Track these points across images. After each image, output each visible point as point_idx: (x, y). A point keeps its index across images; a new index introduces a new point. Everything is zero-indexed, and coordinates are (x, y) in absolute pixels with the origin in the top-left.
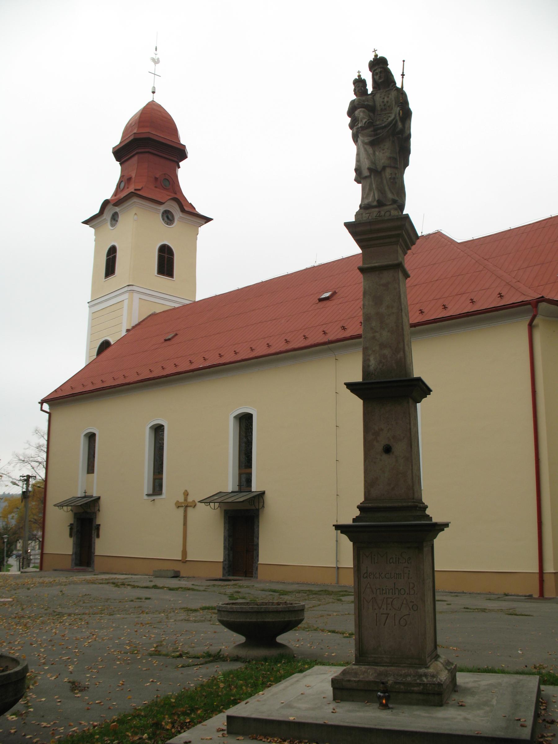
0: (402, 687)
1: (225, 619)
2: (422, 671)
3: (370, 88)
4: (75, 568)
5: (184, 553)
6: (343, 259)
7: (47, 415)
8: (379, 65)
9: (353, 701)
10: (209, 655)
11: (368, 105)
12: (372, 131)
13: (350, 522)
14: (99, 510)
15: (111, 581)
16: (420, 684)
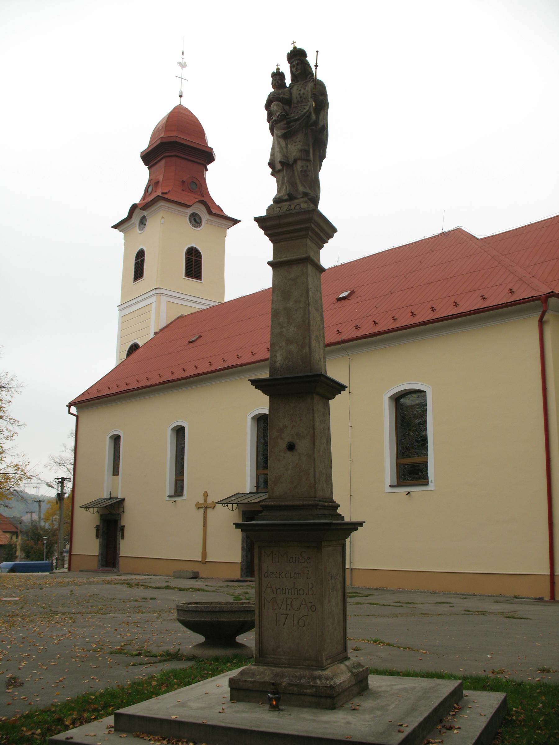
0: (295, 689)
1: (182, 618)
2: (320, 672)
3: (288, 81)
4: (101, 569)
5: (204, 554)
6: (365, 258)
7: (75, 417)
8: (297, 57)
9: (249, 702)
10: (168, 654)
11: (283, 98)
12: (285, 124)
14: (123, 512)
15: (127, 582)
16: (313, 686)
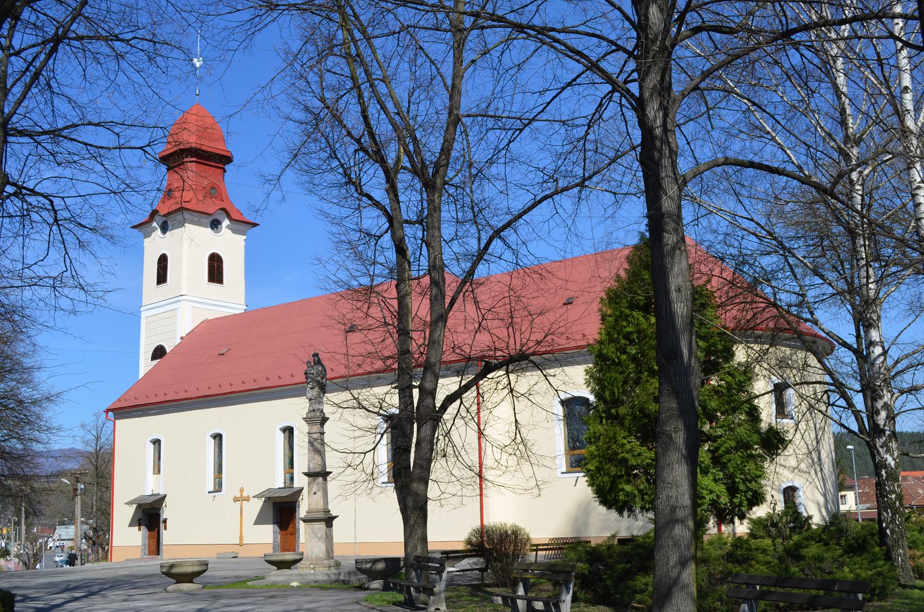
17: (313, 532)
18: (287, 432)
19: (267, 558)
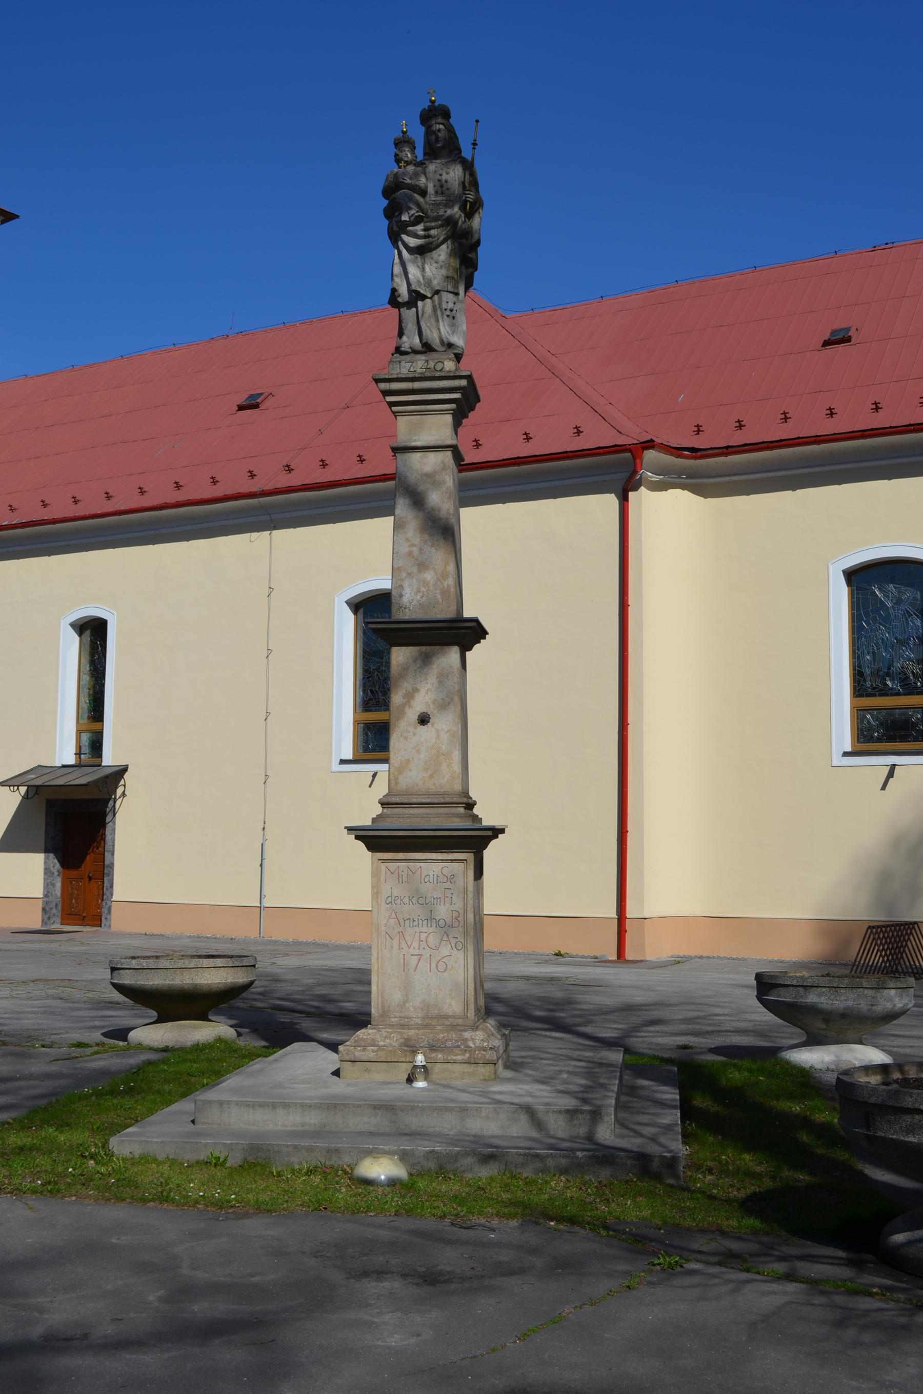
13: (368, 823)
17: (418, 897)
18: (88, 633)
19: (127, 979)
